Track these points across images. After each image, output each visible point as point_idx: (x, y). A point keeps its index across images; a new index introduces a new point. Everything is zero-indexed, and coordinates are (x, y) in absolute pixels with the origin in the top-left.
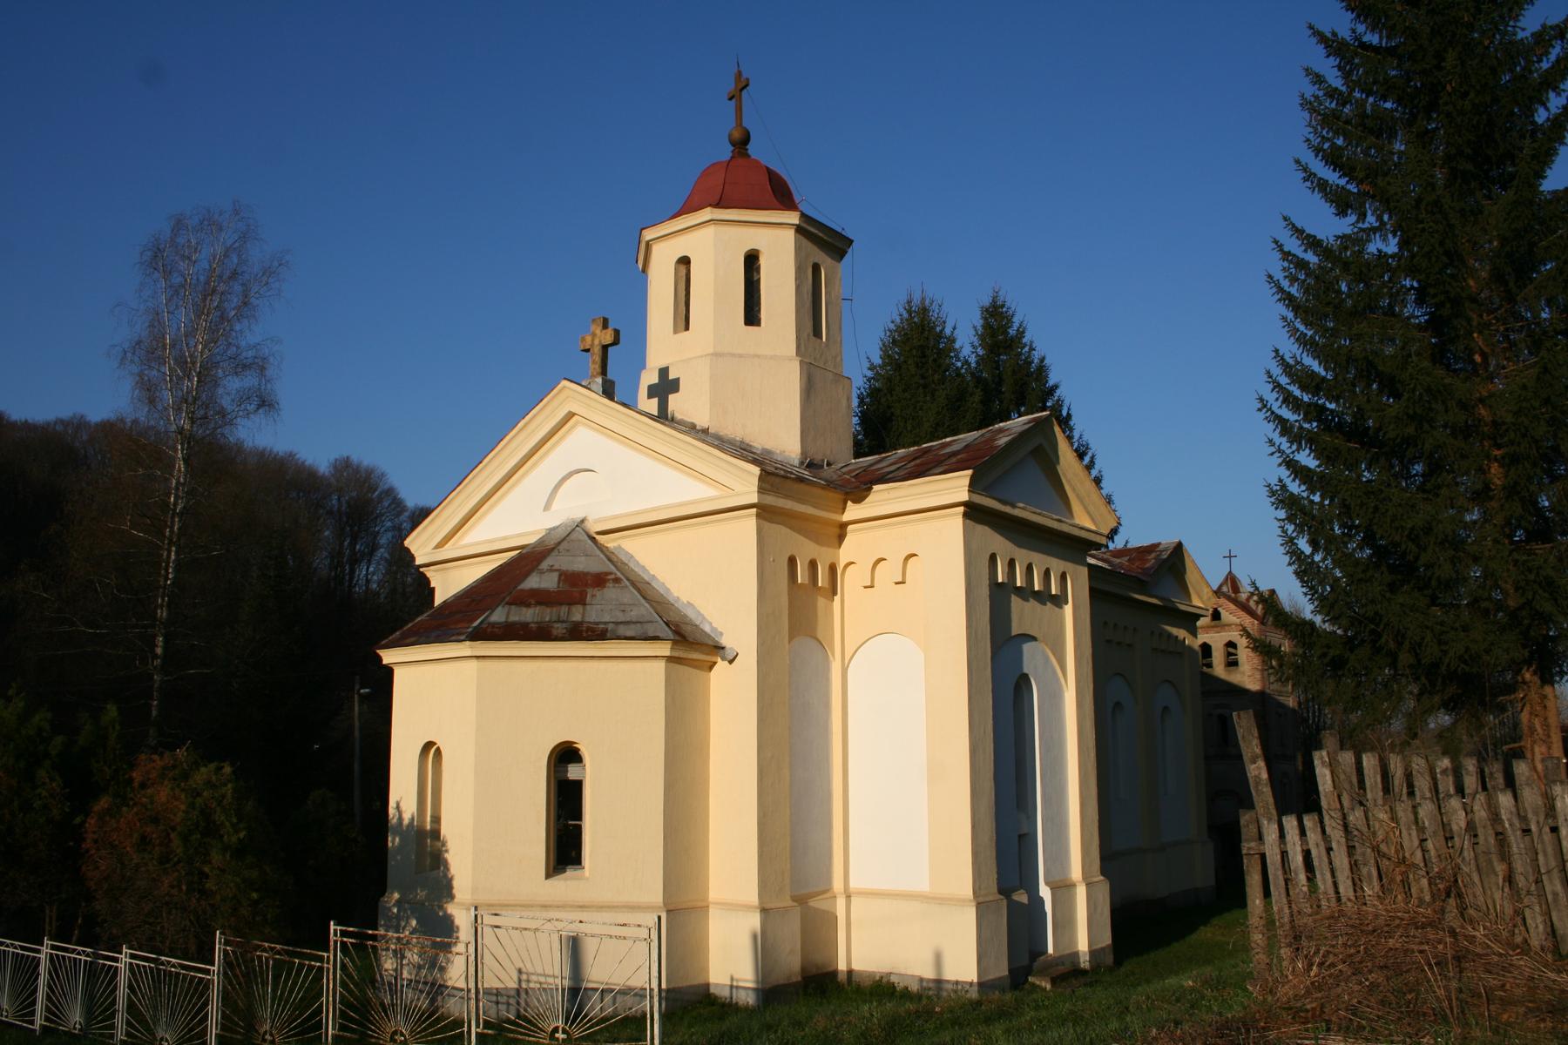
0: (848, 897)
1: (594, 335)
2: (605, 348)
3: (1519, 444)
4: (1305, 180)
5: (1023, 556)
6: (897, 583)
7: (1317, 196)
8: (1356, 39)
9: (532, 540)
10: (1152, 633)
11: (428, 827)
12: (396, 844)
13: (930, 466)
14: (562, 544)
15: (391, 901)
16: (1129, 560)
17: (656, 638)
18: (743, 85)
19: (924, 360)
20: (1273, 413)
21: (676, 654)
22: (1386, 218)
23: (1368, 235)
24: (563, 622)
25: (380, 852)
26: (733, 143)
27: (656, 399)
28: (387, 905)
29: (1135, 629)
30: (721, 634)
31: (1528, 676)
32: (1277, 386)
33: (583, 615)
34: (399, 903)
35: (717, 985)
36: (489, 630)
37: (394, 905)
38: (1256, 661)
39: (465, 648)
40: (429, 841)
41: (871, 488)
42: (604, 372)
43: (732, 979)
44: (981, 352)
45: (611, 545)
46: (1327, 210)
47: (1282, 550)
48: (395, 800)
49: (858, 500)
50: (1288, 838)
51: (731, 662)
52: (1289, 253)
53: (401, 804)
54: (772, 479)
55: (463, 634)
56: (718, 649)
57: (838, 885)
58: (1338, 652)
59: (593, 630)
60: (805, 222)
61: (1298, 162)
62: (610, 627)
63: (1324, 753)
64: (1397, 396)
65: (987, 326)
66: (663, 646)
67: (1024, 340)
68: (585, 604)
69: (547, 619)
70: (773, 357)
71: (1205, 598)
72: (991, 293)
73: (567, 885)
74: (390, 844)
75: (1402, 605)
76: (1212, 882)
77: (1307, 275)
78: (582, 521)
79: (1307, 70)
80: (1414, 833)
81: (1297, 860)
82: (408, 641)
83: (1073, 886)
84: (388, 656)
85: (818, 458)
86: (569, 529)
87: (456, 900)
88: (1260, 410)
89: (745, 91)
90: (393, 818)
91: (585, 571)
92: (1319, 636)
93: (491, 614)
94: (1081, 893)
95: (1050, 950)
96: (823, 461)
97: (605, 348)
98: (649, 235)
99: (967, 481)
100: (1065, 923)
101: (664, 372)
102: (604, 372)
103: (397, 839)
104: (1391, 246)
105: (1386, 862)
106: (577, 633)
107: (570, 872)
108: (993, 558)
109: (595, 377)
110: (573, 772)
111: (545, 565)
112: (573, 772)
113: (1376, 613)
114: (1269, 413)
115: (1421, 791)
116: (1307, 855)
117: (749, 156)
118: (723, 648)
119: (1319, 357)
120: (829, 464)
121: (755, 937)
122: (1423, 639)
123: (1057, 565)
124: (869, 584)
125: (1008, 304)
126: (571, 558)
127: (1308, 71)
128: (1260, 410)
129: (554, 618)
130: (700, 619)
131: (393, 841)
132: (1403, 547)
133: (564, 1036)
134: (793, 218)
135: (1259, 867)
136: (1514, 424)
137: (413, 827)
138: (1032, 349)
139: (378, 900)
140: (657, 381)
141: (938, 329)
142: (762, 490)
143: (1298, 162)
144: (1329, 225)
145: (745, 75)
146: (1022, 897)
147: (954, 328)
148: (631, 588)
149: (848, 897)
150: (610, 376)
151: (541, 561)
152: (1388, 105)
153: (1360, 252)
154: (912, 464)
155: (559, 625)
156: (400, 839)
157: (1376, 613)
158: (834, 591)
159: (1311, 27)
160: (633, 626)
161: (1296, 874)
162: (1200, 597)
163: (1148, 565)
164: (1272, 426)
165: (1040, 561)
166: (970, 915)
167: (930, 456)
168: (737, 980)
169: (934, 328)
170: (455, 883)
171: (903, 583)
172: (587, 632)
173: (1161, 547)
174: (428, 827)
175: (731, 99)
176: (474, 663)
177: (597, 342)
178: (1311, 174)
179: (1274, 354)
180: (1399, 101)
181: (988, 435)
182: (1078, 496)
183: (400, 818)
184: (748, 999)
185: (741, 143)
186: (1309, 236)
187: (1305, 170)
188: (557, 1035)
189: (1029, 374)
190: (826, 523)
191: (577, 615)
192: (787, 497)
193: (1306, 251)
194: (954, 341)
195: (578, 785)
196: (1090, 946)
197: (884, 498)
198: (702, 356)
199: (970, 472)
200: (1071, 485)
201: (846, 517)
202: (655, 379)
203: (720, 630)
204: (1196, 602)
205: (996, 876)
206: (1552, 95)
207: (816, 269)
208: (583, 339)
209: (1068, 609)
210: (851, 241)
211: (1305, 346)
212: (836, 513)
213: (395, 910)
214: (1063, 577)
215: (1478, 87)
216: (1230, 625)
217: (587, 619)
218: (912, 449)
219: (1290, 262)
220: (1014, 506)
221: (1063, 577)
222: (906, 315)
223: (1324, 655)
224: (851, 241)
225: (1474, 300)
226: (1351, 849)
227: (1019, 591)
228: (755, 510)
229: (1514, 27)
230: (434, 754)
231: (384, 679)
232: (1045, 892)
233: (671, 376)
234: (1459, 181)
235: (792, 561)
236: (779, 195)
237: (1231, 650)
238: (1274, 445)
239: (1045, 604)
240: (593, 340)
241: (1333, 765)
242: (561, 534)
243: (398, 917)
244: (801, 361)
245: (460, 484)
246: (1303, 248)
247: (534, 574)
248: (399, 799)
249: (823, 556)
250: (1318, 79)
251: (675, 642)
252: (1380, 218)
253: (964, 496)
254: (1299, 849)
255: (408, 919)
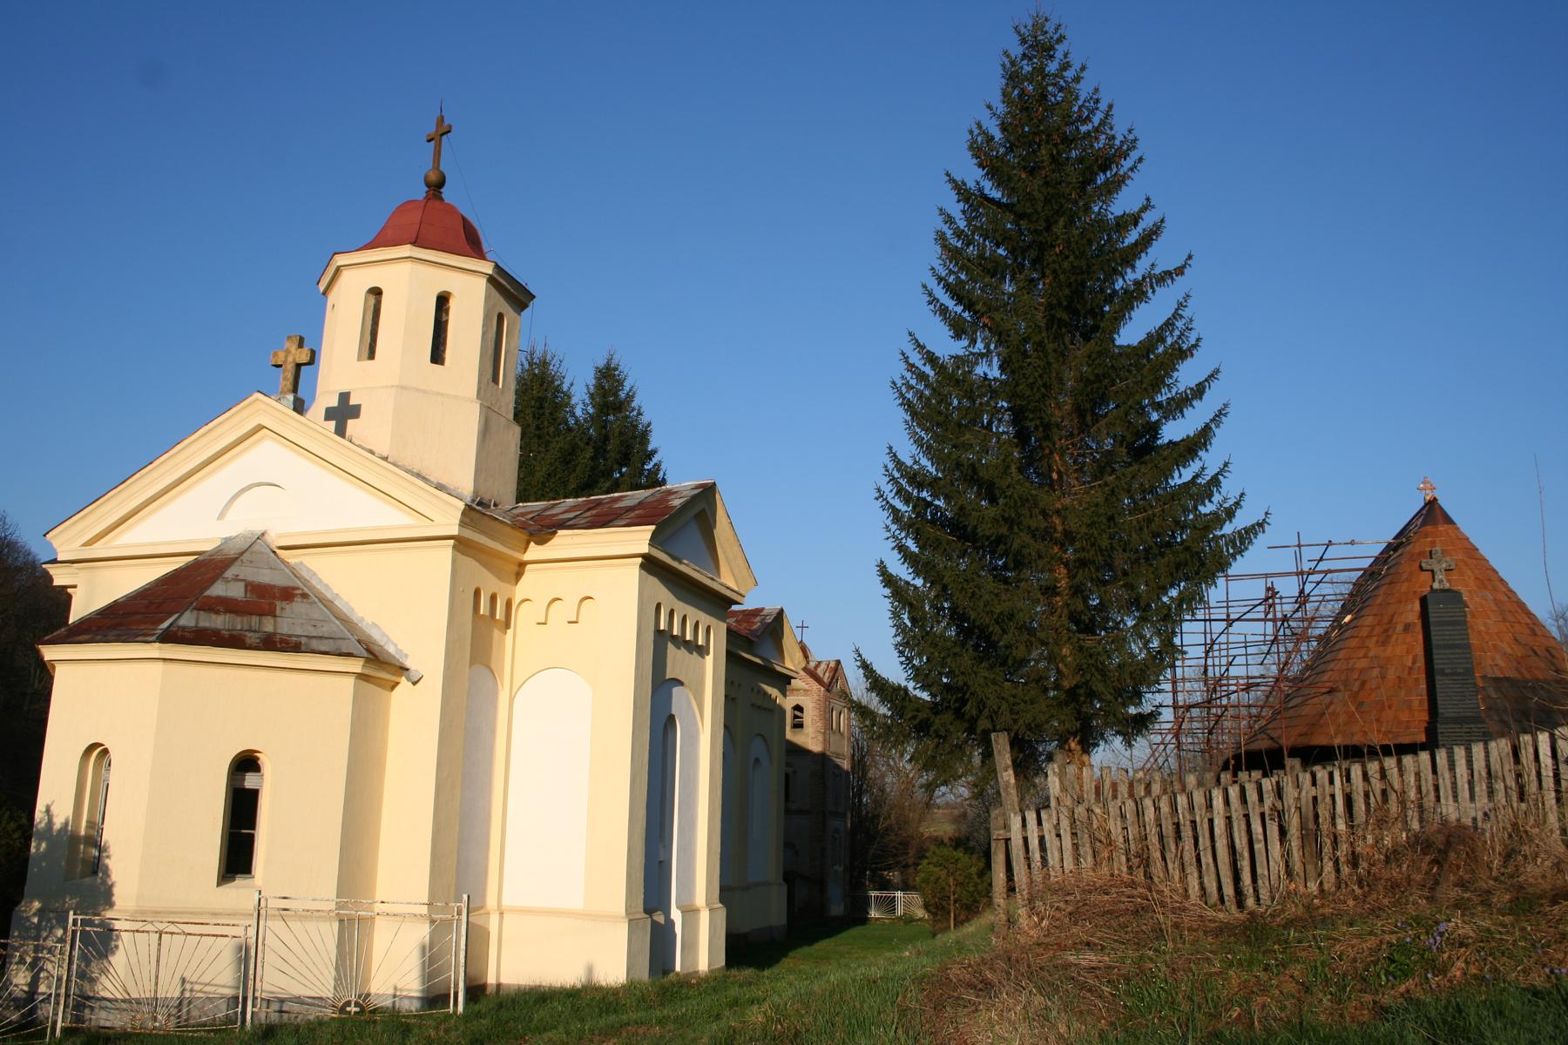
0: (501, 914)
1: (288, 352)
2: (298, 366)
3: (1088, 552)
4: (930, 303)
5: (682, 608)
6: (538, 624)
7: (938, 318)
8: (979, 190)
9: (208, 547)
10: (752, 689)
11: (83, 833)
12: (42, 850)
13: (610, 518)
14: (245, 554)
15: (30, 910)
16: (736, 621)
17: (349, 655)
18: (442, 131)
19: (541, 411)
20: (888, 502)
21: (366, 672)
22: (992, 347)
23: (977, 359)
24: (255, 631)
25: (20, 858)
26: (428, 185)
27: (334, 423)
28: (25, 915)
29: (740, 685)
30: (407, 656)
31: (1073, 745)
32: (893, 480)
33: (275, 628)
34: (40, 912)
35: (378, 995)
36: (180, 633)
37: (34, 915)
38: (819, 724)
39: (155, 650)
40: (82, 847)
41: (555, 533)
42: (295, 390)
43: (395, 988)
44: (591, 410)
45: (292, 561)
46: (945, 331)
47: (891, 623)
48: (45, 804)
49: (542, 542)
50: (1029, 826)
51: (415, 683)
52: (913, 366)
53: (52, 808)
54: (473, 514)
55: (153, 635)
56: (403, 670)
57: (491, 902)
58: (925, 716)
59: (287, 643)
60: (497, 273)
61: (924, 286)
62: (303, 640)
63: (1055, 766)
64: (993, 500)
65: (599, 386)
66: (355, 663)
67: (633, 405)
68: (275, 616)
69: (239, 627)
70: (456, 397)
71: (796, 662)
72: (606, 356)
73: (240, 893)
74: (33, 850)
75: (985, 678)
76: (784, 921)
77: (926, 386)
78: (263, 534)
79: (941, 210)
80: (1119, 823)
81: (1034, 843)
82: (81, 638)
83: (697, 911)
84: (49, 653)
85: (486, 497)
86: (250, 542)
87: (115, 908)
88: (877, 499)
89: (444, 137)
90: (40, 822)
91: (272, 583)
92: (910, 700)
93: (178, 618)
94: (704, 918)
95: (678, 968)
96: (490, 501)
97: (298, 366)
98: (341, 260)
99: (649, 536)
100: (690, 946)
101: (345, 397)
102: (295, 390)
103: (44, 845)
104: (994, 373)
105: (1098, 844)
106: (270, 643)
107: (240, 881)
108: (658, 607)
109: (285, 393)
110: (250, 781)
111: (229, 573)
112: (250, 781)
113: (965, 684)
114: (884, 503)
115: (1122, 794)
116: (1042, 839)
117: (442, 200)
118: (407, 670)
119: (932, 459)
120: (495, 505)
121: (424, 948)
122: (999, 708)
123: (705, 619)
124: (543, 621)
125: (621, 368)
126: (255, 570)
127: (942, 211)
128: (877, 499)
129: (246, 627)
130: (385, 639)
131: (37, 847)
132: (991, 629)
133: (357, 1009)
134: (488, 268)
135: (1004, 849)
136: (1086, 534)
137: (67, 831)
138: (639, 414)
139: (13, 910)
140: (336, 404)
141: (557, 383)
142: (463, 524)
143: (924, 286)
144: (947, 346)
145: (447, 122)
146: (659, 918)
147: (572, 385)
148: (320, 604)
149: (501, 914)
150: (300, 394)
151: (226, 570)
152: (1001, 251)
153: (970, 372)
154: (589, 514)
155: (252, 634)
156: (47, 845)
157: (965, 684)
158: (507, 625)
159: (948, 175)
160: (326, 641)
161: (1033, 853)
162: (792, 661)
163: (754, 627)
164: (886, 514)
165: (694, 614)
166: (622, 930)
167: (605, 508)
168: (401, 990)
169: (553, 382)
170: (116, 890)
171: (545, 624)
172: (281, 643)
173: (765, 612)
174: (83, 833)
175: (429, 141)
176: (160, 665)
177: (290, 359)
178: (935, 299)
179: (888, 451)
180: (1012, 251)
181: (658, 495)
182: (727, 558)
183: (50, 823)
184: (414, 1006)
185: (436, 186)
186: (928, 352)
187: (930, 294)
188: (348, 1009)
189: (634, 437)
190: (508, 559)
191: (268, 626)
192: (482, 532)
193: (925, 364)
194: (569, 397)
195: (254, 794)
196: (709, 966)
197: (567, 542)
198: (387, 387)
199: (653, 527)
200: (722, 547)
201: (527, 557)
202: (334, 403)
203: (405, 652)
204: (788, 664)
205: (642, 897)
206: (1129, 270)
207: (500, 317)
208: (275, 354)
209: (709, 659)
210: (534, 297)
211: (922, 447)
212: (518, 551)
213: (35, 920)
214: (708, 629)
215: (1077, 253)
216: (798, 690)
217: (279, 631)
218: (580, 499)
219: (913, 373)
220: (680, 562)
221: (708, 629)
222: (526, 366)
223: (914, 717)
224: (534, 297)
225: (1058, 426)
226: (1074, 834)
227: (674, 638)
228: (452, 541)
229: (1106, 210)
230: (100, 752)
231: (45, 674)
232: (676, 915)
233: (353, 402)
234: (1055, 326)
235: (477, 593)
236: (470, 243)
237: (798, 713)
238: (889, 531)
239: (692, 653)
240: (286, 357)
241: (1062, 775)
242: (241, 545)
243: (38, 927)
244: (481, 405)
245: (124, 482)
246: (923, 362)
247: (219, 582)
248: (49, 803)
249: (503, 590)
250: (949, 220)
251: (367, 660)
252: (987, 346)
253: (645, 549)
254: (1036, 835)
255: (52, 928)
